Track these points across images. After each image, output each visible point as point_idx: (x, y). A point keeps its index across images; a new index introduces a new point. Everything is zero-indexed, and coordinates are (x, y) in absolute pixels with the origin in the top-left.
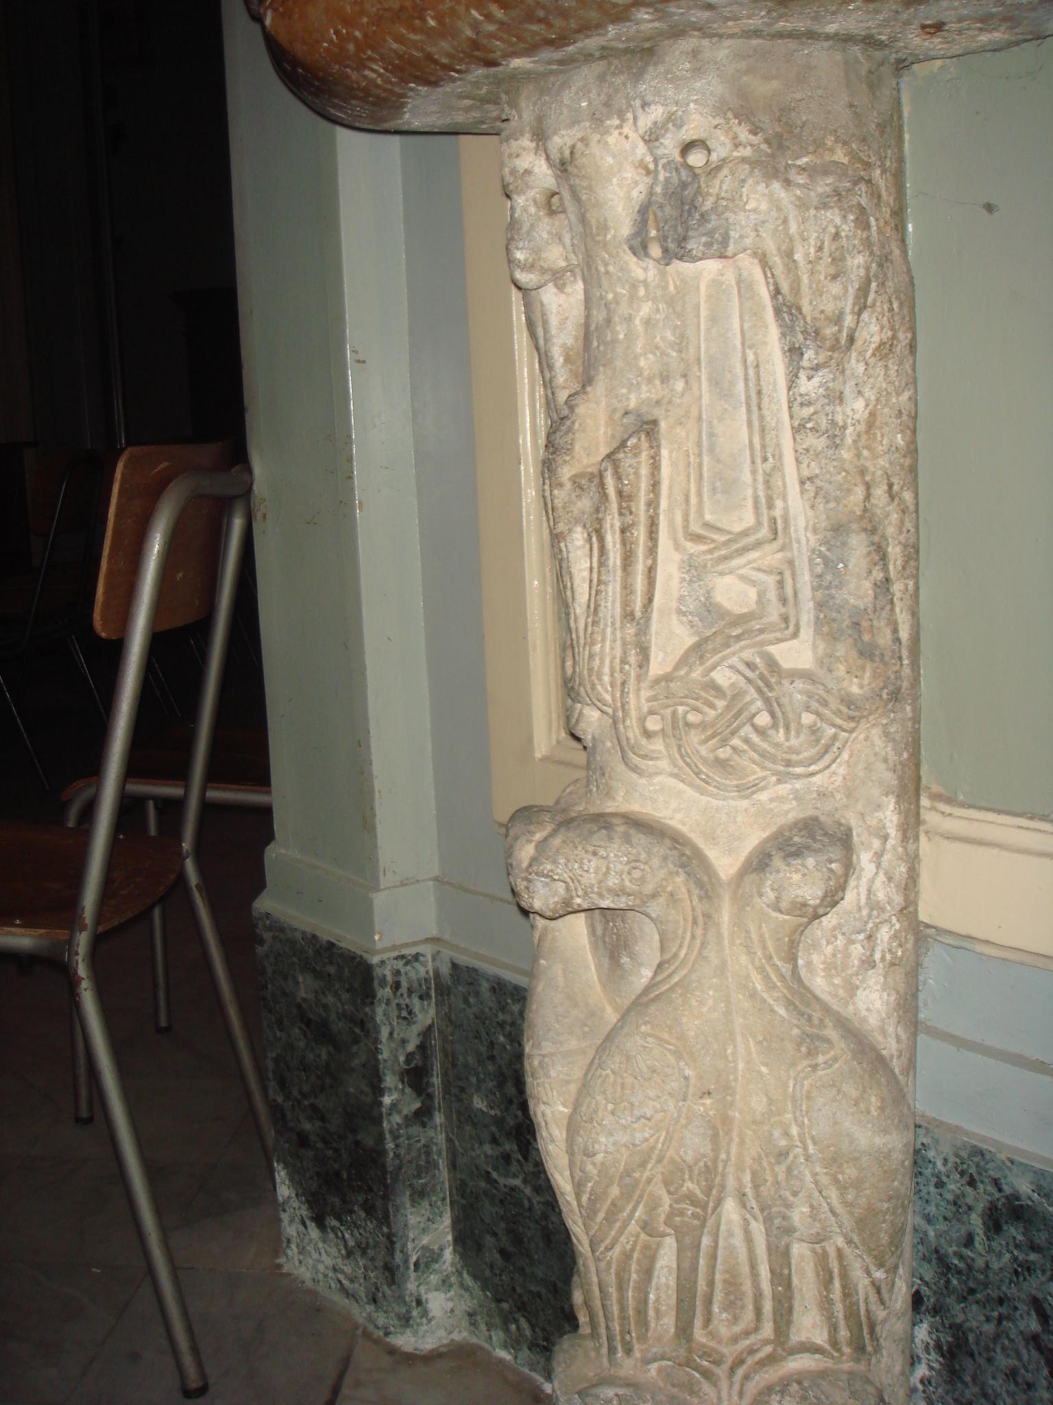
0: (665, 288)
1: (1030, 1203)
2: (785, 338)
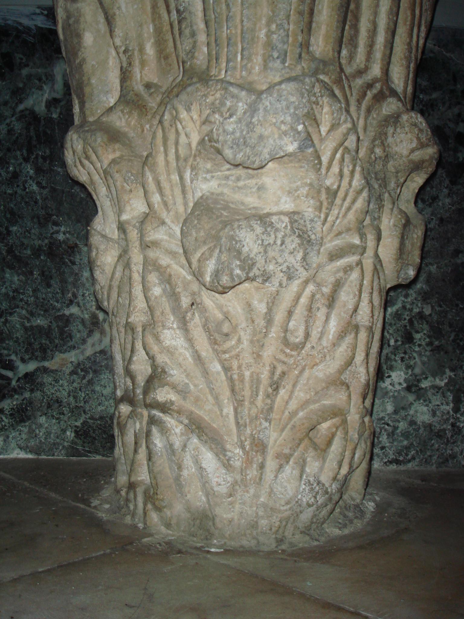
1: (432, 55)
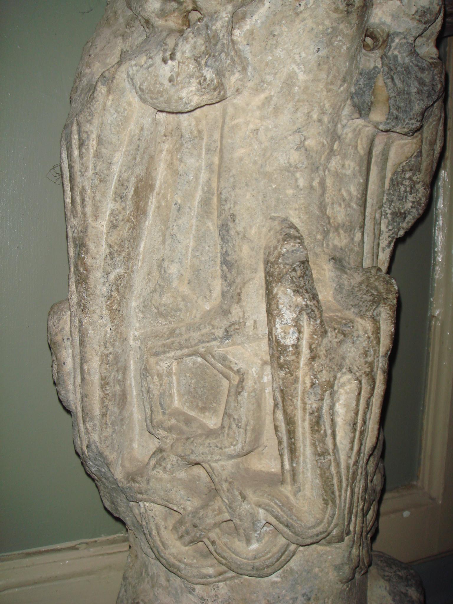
0: (356, 147)
2: (390, 205)
